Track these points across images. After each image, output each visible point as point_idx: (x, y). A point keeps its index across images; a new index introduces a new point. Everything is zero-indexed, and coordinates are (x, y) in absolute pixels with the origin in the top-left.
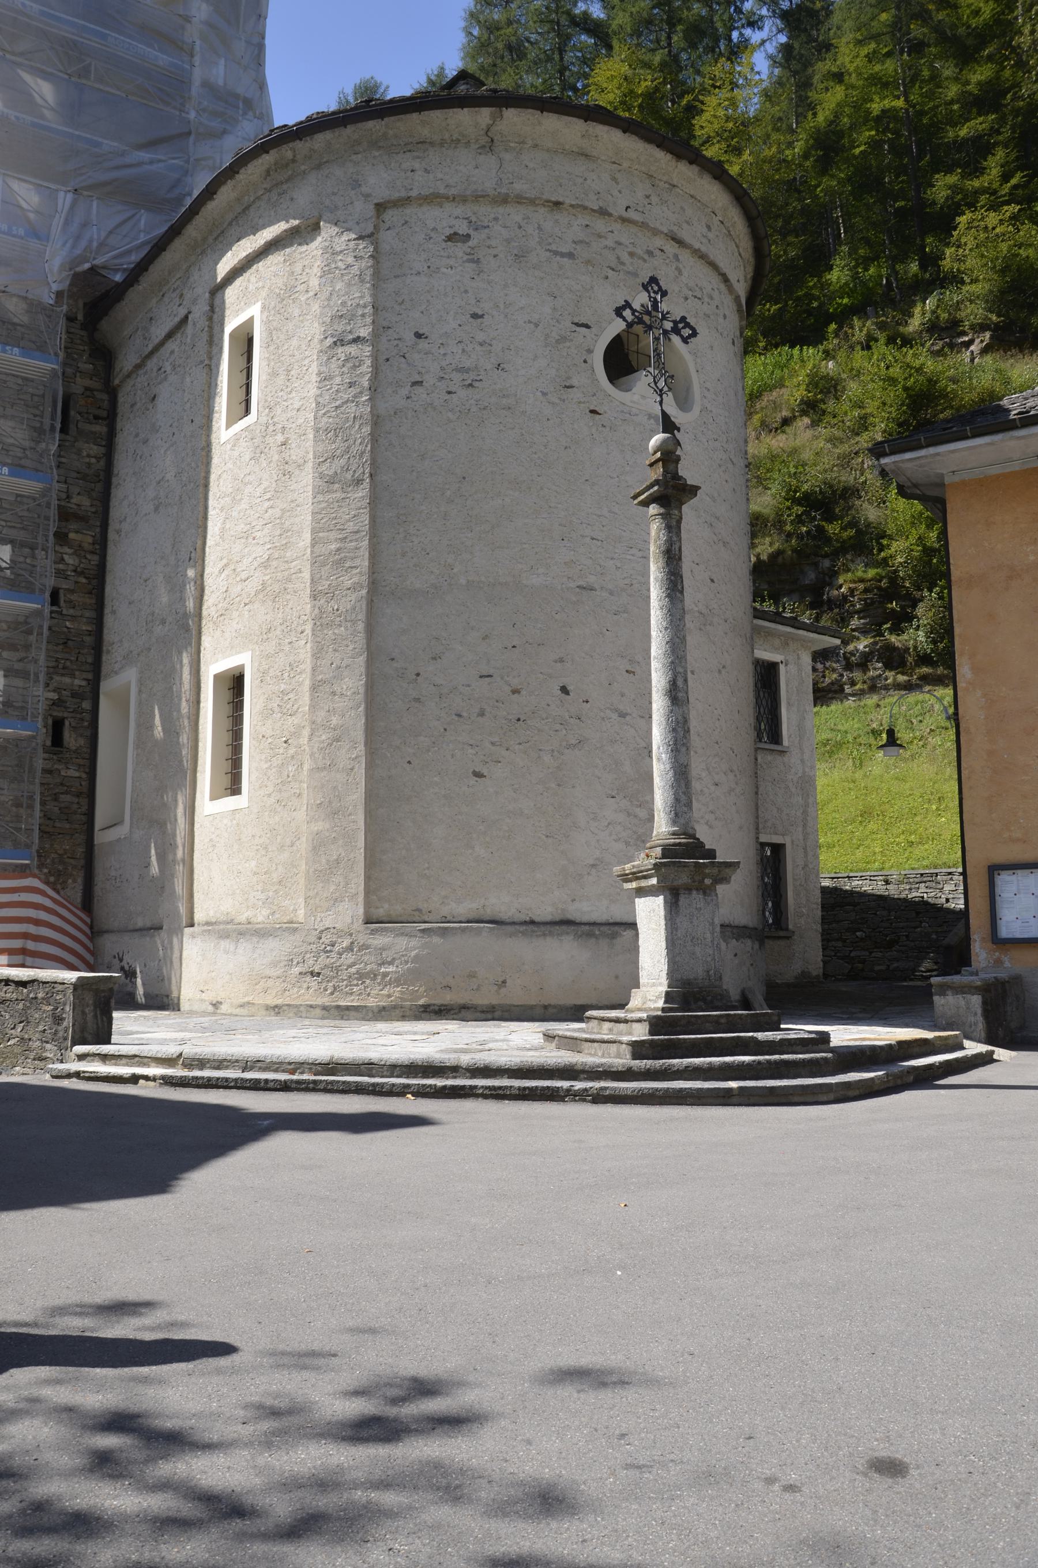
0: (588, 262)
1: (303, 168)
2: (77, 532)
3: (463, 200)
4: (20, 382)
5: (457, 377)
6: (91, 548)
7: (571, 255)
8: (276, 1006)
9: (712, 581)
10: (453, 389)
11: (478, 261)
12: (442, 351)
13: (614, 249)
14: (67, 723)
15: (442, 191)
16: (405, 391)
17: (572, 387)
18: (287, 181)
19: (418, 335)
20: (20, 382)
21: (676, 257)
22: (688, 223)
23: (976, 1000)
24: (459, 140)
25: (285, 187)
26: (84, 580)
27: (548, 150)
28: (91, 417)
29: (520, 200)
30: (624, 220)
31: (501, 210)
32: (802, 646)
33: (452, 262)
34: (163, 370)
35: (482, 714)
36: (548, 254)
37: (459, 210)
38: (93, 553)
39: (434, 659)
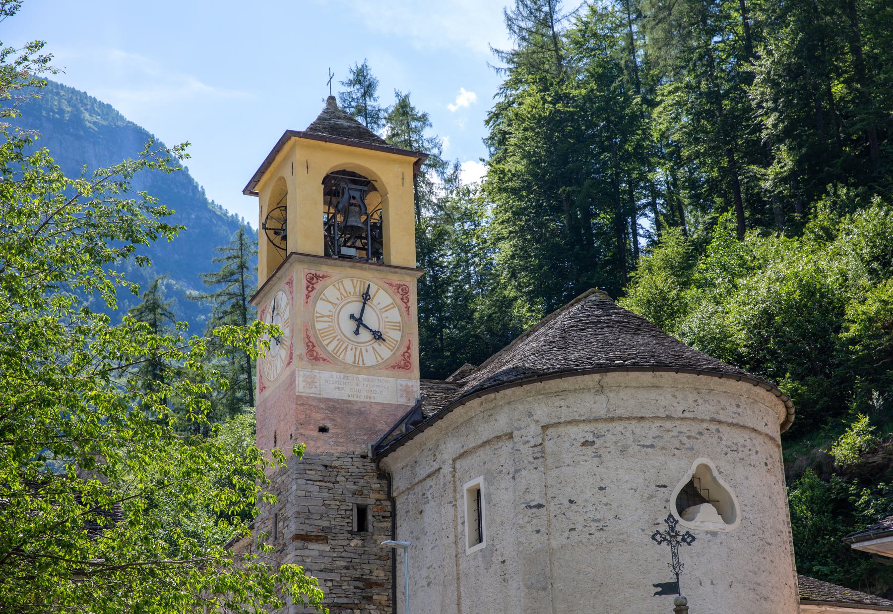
0: (663, 448)
1: (500, 403)
2: (378, 594)
3: (588, 421)
4: (338, 503)
5: (594, 525)
6: (386, 603)
7: (652, 446)
10: (592, 532)
11: (600, 456)
12: (585, 510)
13: (677, 437)
16: (566, 534)
17: (658, 524)
18: (493, 409)
19: (571, 502)
20: (338, 503)
21: (718, 431)
22: (723, 409)
24: (584, 389)
25: (492, 412)
27: (634, 387)
28: (381, 518)
29: (620, 419)
30: (682, 419)
33: (586, 458)
34: (426, 496)
36: (639, 447)
37: (588, 427)
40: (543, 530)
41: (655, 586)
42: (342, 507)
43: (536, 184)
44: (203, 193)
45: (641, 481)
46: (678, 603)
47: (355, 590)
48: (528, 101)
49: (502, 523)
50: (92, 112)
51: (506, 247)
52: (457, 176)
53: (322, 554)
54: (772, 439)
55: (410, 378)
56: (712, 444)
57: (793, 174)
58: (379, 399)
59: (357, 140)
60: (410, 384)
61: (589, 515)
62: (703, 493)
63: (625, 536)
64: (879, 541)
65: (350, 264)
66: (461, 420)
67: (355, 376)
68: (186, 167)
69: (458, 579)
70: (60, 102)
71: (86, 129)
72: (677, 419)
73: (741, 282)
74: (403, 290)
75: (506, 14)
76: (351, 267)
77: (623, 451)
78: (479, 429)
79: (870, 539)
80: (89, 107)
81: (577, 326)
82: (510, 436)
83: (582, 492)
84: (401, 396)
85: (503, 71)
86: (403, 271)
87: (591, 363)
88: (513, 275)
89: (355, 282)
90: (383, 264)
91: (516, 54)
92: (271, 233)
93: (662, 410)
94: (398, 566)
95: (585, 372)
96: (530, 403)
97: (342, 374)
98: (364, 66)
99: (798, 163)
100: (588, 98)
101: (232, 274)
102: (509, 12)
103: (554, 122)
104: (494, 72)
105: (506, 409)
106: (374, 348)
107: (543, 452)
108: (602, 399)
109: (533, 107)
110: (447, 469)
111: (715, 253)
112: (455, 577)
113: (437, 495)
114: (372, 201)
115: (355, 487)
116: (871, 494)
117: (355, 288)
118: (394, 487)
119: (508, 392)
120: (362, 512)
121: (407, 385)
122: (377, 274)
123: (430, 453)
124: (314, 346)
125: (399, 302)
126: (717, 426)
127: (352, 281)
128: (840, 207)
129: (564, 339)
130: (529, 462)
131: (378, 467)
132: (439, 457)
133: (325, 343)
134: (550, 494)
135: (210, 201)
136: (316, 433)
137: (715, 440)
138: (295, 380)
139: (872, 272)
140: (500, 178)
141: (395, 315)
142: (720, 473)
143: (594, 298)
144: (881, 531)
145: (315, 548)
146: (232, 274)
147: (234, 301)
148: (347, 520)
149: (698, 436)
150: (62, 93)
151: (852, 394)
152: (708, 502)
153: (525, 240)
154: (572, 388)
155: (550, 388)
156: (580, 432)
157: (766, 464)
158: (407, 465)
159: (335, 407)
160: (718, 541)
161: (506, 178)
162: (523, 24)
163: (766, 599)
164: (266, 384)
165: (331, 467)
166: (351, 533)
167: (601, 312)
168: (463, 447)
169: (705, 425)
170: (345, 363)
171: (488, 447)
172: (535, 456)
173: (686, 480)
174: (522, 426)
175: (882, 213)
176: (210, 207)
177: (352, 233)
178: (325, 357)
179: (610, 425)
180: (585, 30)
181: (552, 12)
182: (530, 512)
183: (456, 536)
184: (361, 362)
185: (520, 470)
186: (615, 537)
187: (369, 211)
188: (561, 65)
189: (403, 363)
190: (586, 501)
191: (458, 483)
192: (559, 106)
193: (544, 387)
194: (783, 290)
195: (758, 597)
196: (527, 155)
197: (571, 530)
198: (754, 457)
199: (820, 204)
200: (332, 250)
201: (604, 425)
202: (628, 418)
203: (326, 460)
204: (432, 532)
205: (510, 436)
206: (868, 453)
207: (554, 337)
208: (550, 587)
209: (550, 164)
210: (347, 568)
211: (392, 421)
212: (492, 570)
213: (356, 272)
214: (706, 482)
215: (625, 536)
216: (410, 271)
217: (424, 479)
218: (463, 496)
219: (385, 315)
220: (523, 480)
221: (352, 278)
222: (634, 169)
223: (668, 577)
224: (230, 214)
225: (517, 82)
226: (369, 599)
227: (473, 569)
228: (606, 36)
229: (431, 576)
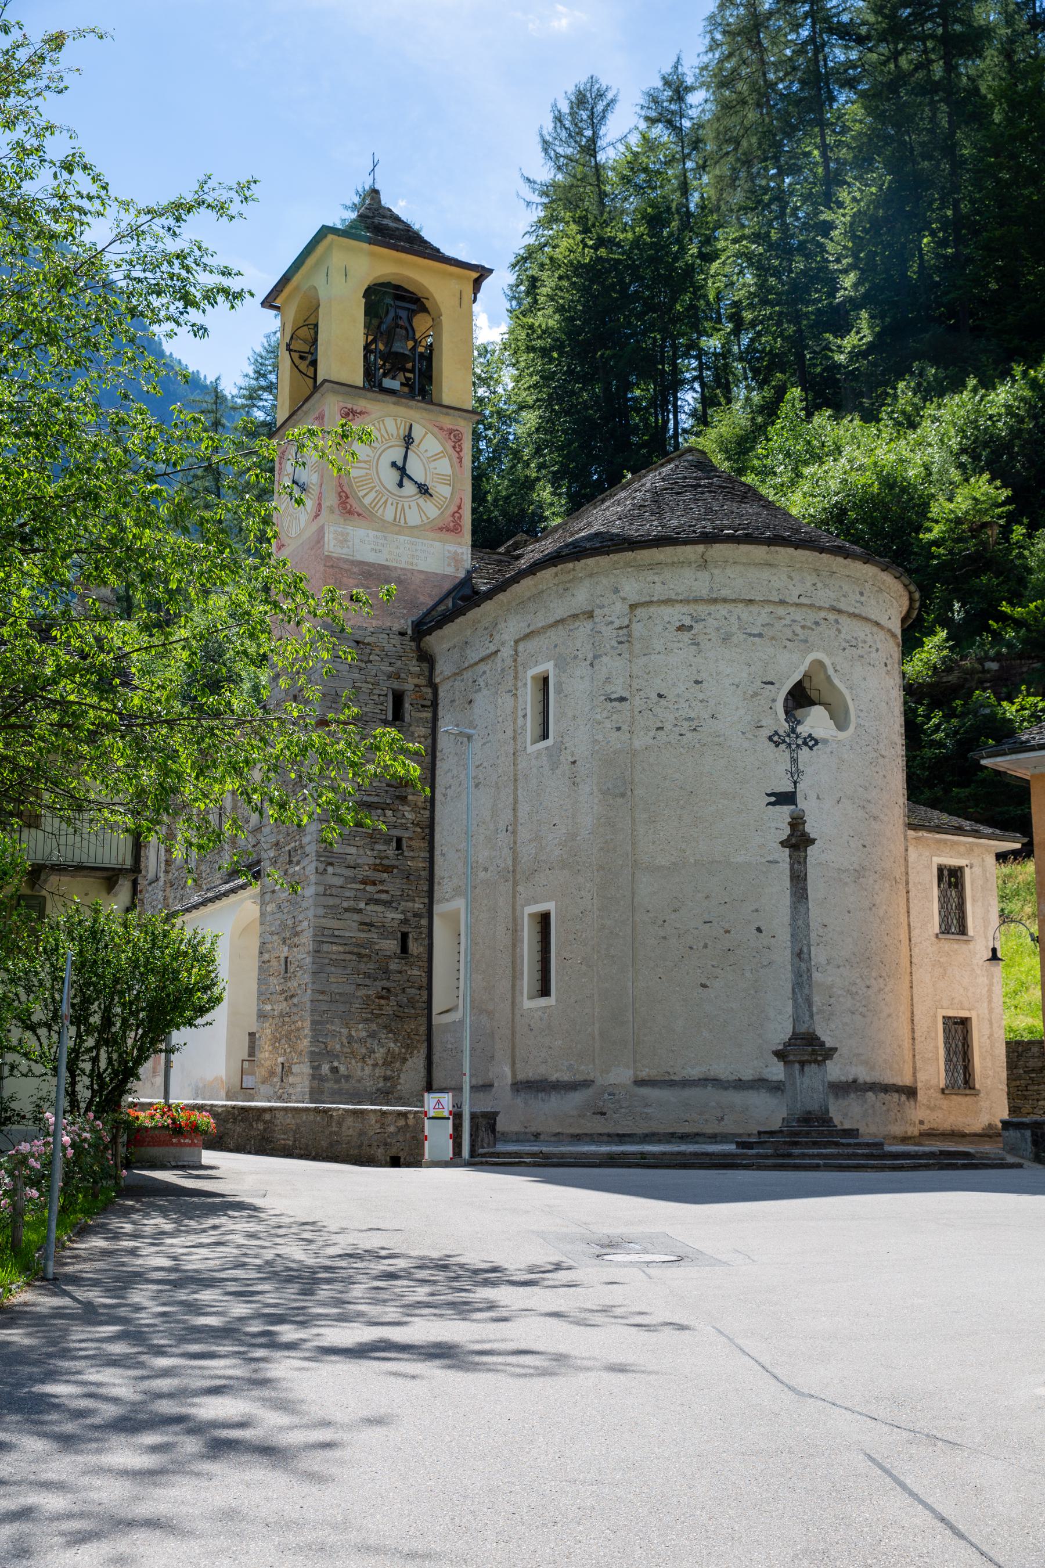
0: (773, 638)
3: (686, 601)
4: (371, 686)
5: (686, 724)
6: (423, 805)
7: (760, 635)
8: (578, 1135)
9: (864, 846)
11: (698, 644)
12: (676, 707)
14: (411, 936)
15: (674, 597)
18: (570, 581)
19: (660, 696)
20: (371, 686)
21: (837, 622)
22: (844, 596)
23: (1028, 1133)
24: (683, 562)
25: (568, 585)
26: (419, 830)
27: (744, 564)
29: (725, 600)
30: (797, 605)
31: (713, 607)
32: (987, 850)
33: (681, 645)
35: (706, 946)
37: (685, 609)
38: (425, 809)
39: (675, 911)
40: (625, 727)
41: (768, 795)
42: (375, 692)
43: (569, 345)
45: (745, 675)
46: (795, 815)
47: (387, 788)
48: (565, 243)
49: (574, 717)
51: (531, 418)
54: (893, 635)
55: (459, 544)
56: (829, 637)
57: (871, 347)
59: (407, 245)
60: (460, 551)
61: (680, 712)
62: (814, 695)
63: (722, 739)
64: (1014, 757)
65: (394, 399)
66: (528, 594)
67: (396, 536)
69: (516, 780)
72: (792, 605)
73: (807, 471)
74: (454, 436)
75: (541, 135)
76: (394, 404)
77: (726, 639)
78: (551, 605)
79: (1005, 754)
81: (672, 489)
82: (590, 615)
83: (674, 685)
84: (449, 565)
85: (534, 206)
86: (457, 413)
87: (694, 532)
88: (538, 451)
89: (399, 422)
90: (431, 402)
91: (554, 185)
92: (295, 355)
93: (775, 593)
94: (438, 764)
95: (686, 542)
96: (616, 576)
97: (379, 534)
99: (878, 336)
100: (637, 242)
102: (545, 132)
104: (523, 205)
105: (587, 582)
106: (418, 505)
107: (630, 636)
108: (704, 575)
109: (571, 251)
110: (506, 652)
111: (778, 435)
112: (512, 778)
113: (492, 682)
114: (421, 323)
115: (390, 669)
116: (943, 717)
117: (398, 429)
118: (437, 672)
119: (591, 561)
120: (398, 698)
121: (456, 552)
122: (425, 414)
123: (486, 632)
124: (347, 497)
125: (451, 451)
126: (836, 617)
127: (396, 420)
128: (925, 391)
129: (657, 501)
130: (612, 647)
131: (419, 647)
132: (497, 637)
133: (361, 494)
134: (635, 686)
135: (168, 354)
137: (832, 632)
138: (323, 537)
139: (961, 466)
140: (528, 335)
141: (444, 466)
142: (836, 671)
143: (690, 458)
144: (1018, 745)
148: (381, 707)
149: (814, 627)
151: (930, 604)
152: (820, 704)
153: (553, 410)
154: (669, 561)
155: (642, 559)
156: (675, 614)
157: (886, 665)
158: (455, 647)
160: (829, 750)
161: (535, 336)
162: (560, 150)
163: (875, 818)
165: (364, 643)
167: (700, 474)
168: (529, 626)
169: (823, 614)
170: (384, 521)
171: (560, 627)
172: (620, 639)
173: (796, 677)
174: (606, 604)
175: (977, 398)
177: (395, 362)
178: (360, 512)
179: (713, 608)
180: (634, 164)
181: (593, 140)
182: (609, 705)
183: (515, 731)
184: (402, 520)
185: (600, 656)
186: (709, 739)
187: (417, 336)
188: (603, 205)
189: (452, 524)
190: (678, 695)
191: (520, 669)
192: (602, 252)
193: (635, 559)
194: (861, 479)
195: (867, 816)
196: (560, 309)
197: (658, 729)
198: (874, 655)
199: (901, 385)
200: (372, 381)
201: (705, 607)
202: (734, 601)
204: (484, 725)
205: (590, 615)
206: (943, 671)
207: (644, 500)
208: (629, 793)
209: (586, 322)
211: (437, 593)
212: (559, 772)
213: (401, 410)
214: (818, 681)
215: (722, 739)
216: (464, 414)
217: (476, 664)
218: (526, 684)
219: (432, 465)
220: (604, 668)
221: (395, 417)
222: (683, 335)
223: (785, 786)
225: (551, 220)
227: (535, 770)
228: (658, 172)
229: (480, 776)
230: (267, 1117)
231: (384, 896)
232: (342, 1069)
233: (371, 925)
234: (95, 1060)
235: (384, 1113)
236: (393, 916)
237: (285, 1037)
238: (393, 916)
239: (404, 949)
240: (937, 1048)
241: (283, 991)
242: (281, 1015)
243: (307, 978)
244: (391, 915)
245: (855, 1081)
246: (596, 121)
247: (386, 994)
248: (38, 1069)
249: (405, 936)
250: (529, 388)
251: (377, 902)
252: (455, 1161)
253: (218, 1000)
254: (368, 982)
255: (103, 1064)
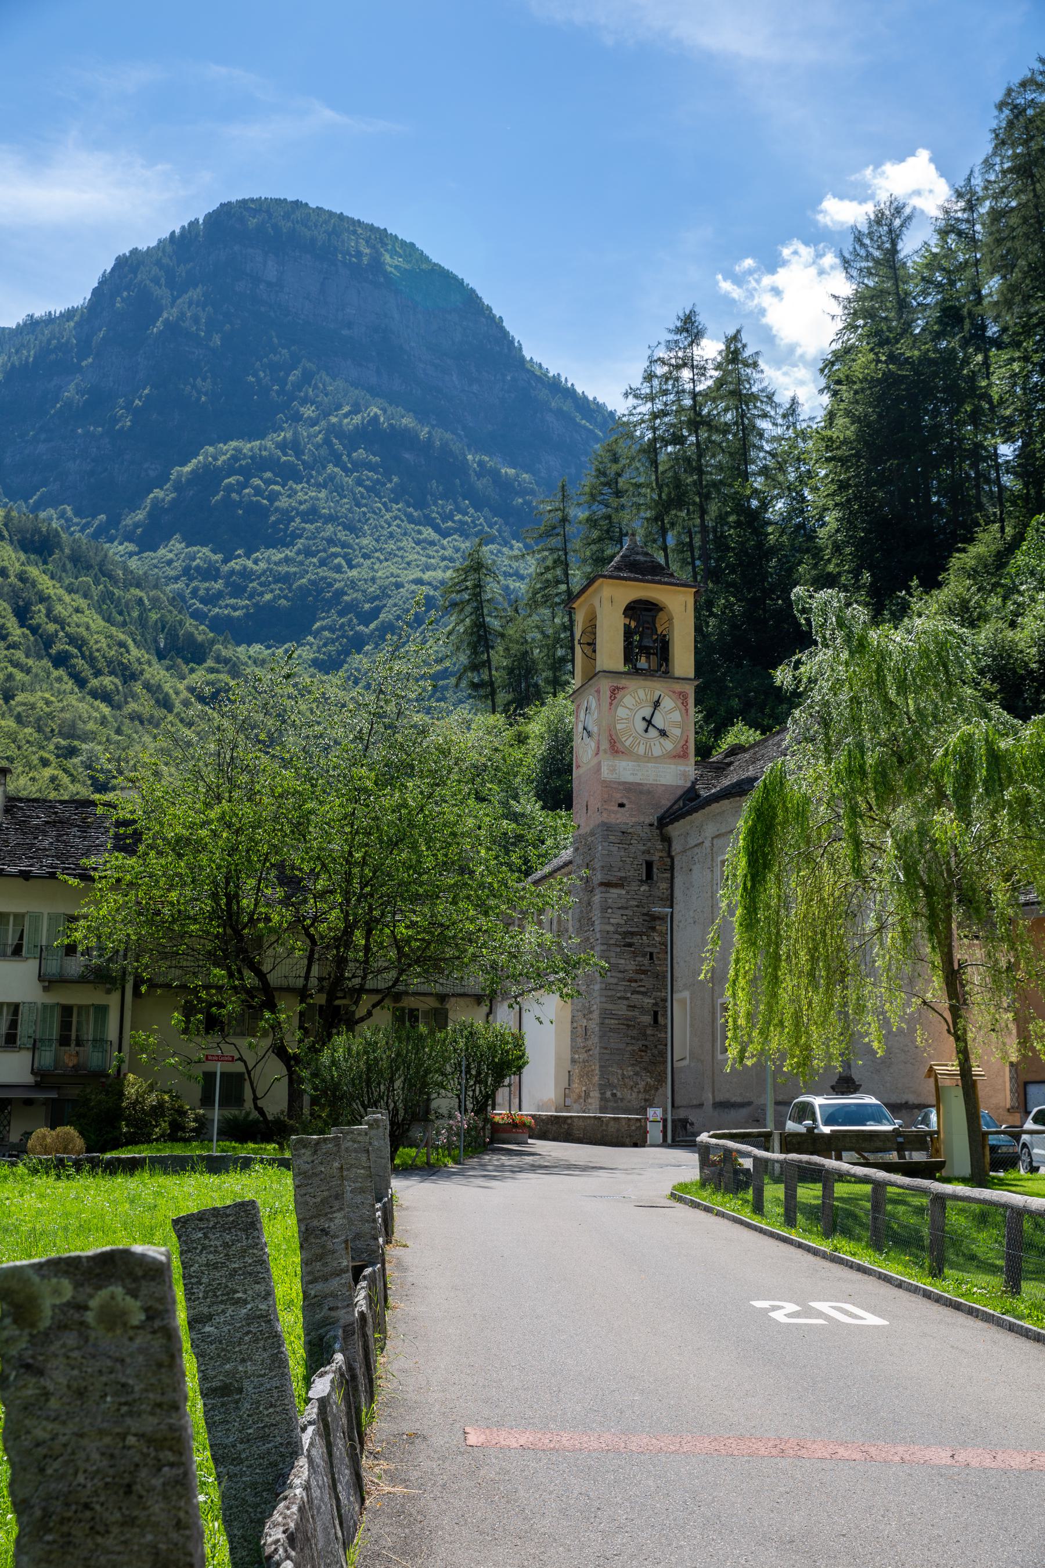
44: (520, 349)
50: (393, 253)
52: (794, 410)
53: (619, 896)
58: (663, 781)
68: (500, 317)
70: (357, 243)
71: (386, 275)
74: (683, 696)
80: (390, 247)
98: (693, 312)
101: (554, 528)
103: (889, 381)
110: (707, 844)
125: (680, 705)
131: (661, 833)
135: (528, 359)
136: (616, 808)
141: (676, 716)
145: (615, 891)
146: (554, 528)
147: (555, 556)
150: (360, 231)
159: (631, 788)
164: (581, 764)
166: (641, 881)
176: (528, 366)
180: (933, 262)
203: (624, 828)
210: (637, 906)
211: (673, 798)
213: (648, 683)
219: (669, 716)
221: (644, 688)
224: (551, 374)
225: (851, 327)
226: (653, 929)
230: (569, 1121)
231: (642, 989)
232: (619, 1094)
233: (634, 1007)
234: (474, 1091)
235: (629, 1119)
236: (648, 1001)
237: (586, 1075)
238: (648, 1001)
239: (656, 1021)
240: (1005, 1082)
241: (584, 1047)
242: (584, 1062)
243: (596, 1040)
244: (647, 1000)
245: (906, 1103)
246: (894, 236)
247: (645, 1049)
248: (450, 1095)
249: (656, 1014)
250: (828, 495)
251: (638, 993)
252: (664, 1144)
253: (527, 1062)
254: (633, 1041)
255: (477, 1093)
